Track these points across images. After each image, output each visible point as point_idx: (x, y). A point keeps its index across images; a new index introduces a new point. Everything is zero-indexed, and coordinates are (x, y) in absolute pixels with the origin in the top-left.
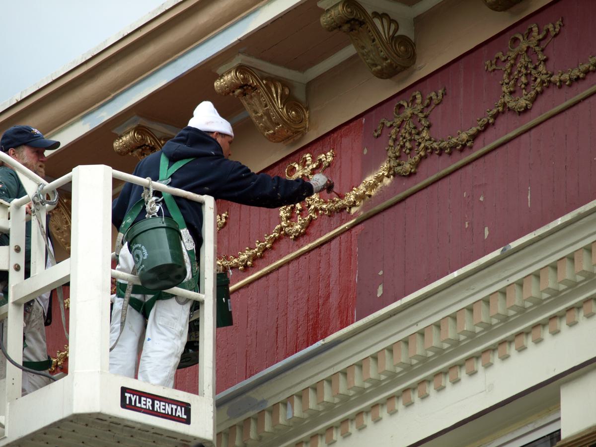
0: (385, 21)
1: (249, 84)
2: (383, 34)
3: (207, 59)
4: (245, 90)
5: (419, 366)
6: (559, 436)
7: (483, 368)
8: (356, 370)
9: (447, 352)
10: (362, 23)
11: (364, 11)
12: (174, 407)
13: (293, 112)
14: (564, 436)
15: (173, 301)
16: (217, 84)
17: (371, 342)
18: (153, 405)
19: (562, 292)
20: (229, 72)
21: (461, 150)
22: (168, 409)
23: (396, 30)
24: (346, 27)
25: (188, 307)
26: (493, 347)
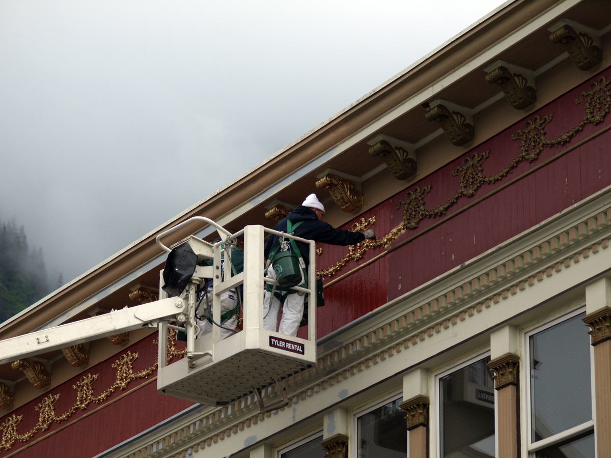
6: (490, 358)
12: (296, 346)
14: (492, 358)
15: (296, 295)
18: (285, 345)
22: (293, 347)
25: (303, 297)
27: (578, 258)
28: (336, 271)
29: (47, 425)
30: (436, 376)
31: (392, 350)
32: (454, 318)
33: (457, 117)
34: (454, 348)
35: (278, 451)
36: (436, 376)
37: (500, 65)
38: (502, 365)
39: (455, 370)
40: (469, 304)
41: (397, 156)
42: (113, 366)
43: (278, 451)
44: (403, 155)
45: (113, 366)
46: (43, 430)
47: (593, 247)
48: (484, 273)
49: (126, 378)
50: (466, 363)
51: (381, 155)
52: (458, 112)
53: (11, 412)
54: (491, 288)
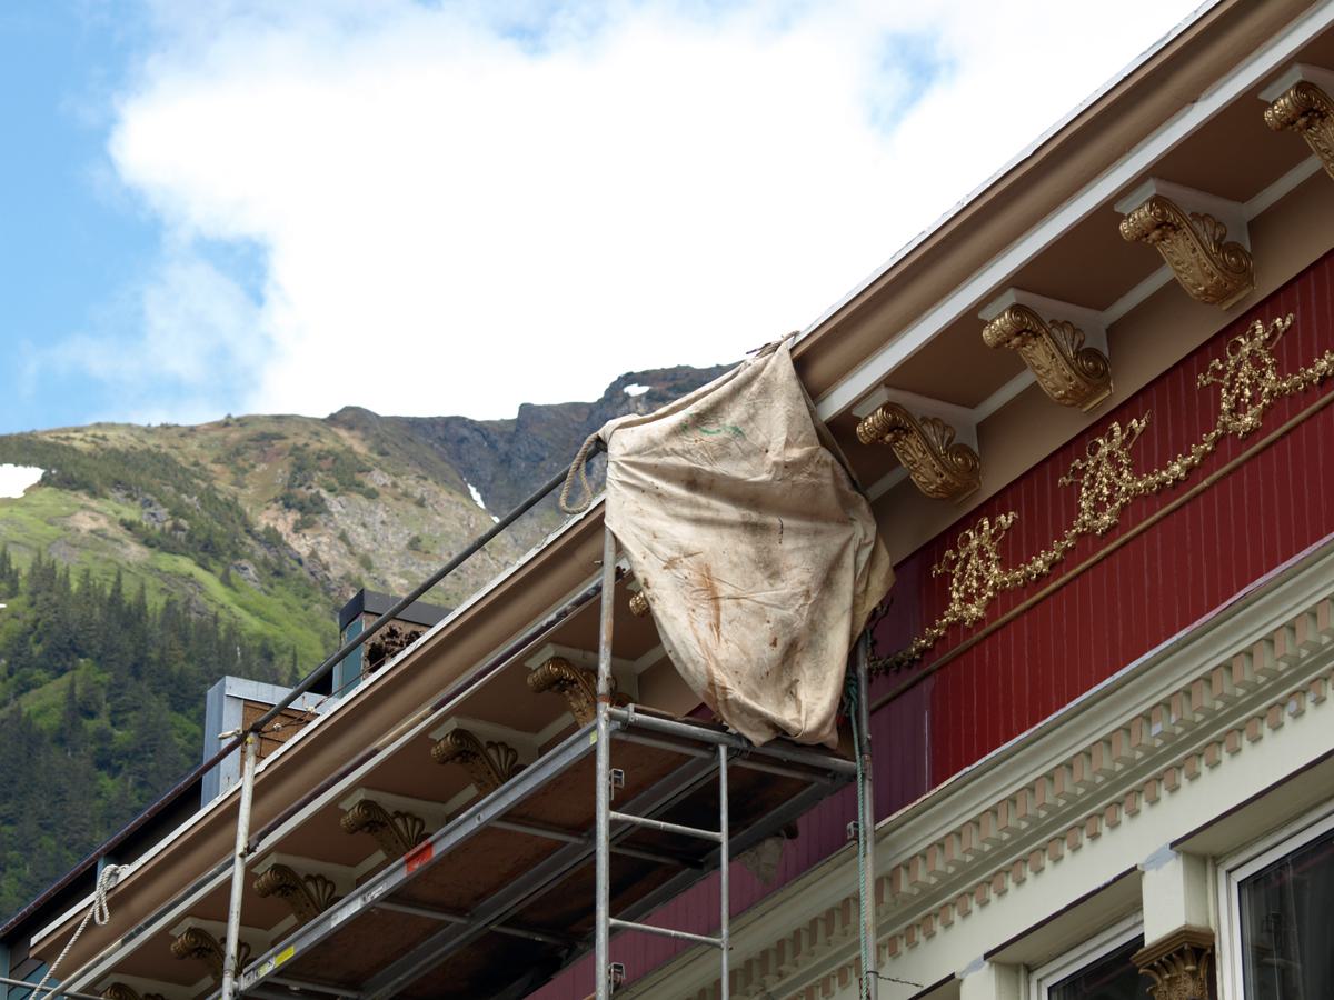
0: (319, 883)
1: (1169, 221)
2: (496, 760)
3: (1129, 179)
4: (1023, 338)
5: (1313, 658)
6: (1143, 942)
7: (1187, 780)
8: (920, 860)
9: (1307, 662)
10: (475, 755)
11: (385, 814)
13: (960, 460)
14: (1148, 941)
16: (1268, 114)
17: (1084, 734)
19: (1282, 673)
20: (1001, 315)
21: (910, 667)
23: (1081, 343)
24: (367, 829)
26: (1007, 869)
27: (1077, 839)
28: (1053, 565)
29: (1182, 467)
30: (1229, 872)
31: (1323, 685)
32: (1212, 747)
33: (405, 821)
34: (1052, 923)
35: (1039, 981)
36: (1229, 872)
37: (552, 654)
38: (1160, 962)
39: (1108, 951)
40: (1229, 722)
41: (398, 831)
42: (1204, 380)
43: (1039, 981)
44: (324, 890)
45: (1204, 380)
46: (1099, 533)
47: (1269, 715)
48: (969, 821)
49: (1111, 499)
50: (1114, 942)
51: (458, 759)
52: (1207, 215)
53: (1242, 317)
54: (1262, 690)
